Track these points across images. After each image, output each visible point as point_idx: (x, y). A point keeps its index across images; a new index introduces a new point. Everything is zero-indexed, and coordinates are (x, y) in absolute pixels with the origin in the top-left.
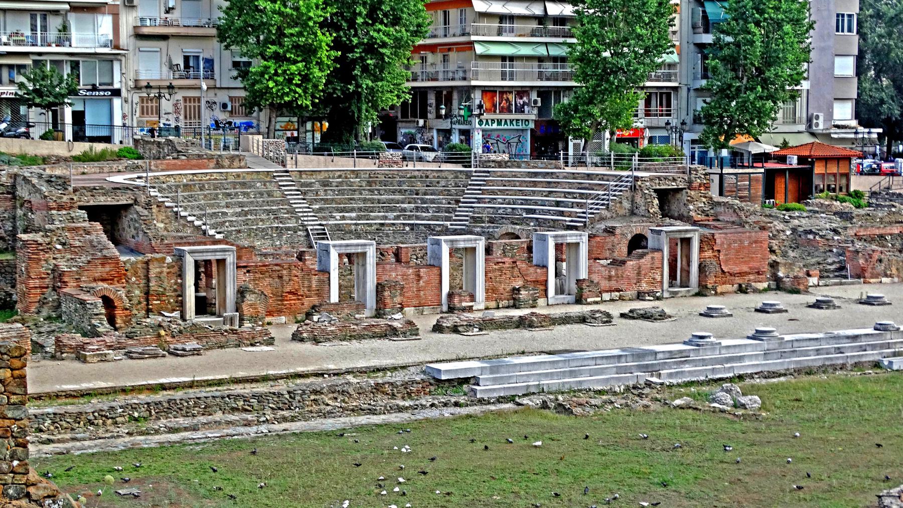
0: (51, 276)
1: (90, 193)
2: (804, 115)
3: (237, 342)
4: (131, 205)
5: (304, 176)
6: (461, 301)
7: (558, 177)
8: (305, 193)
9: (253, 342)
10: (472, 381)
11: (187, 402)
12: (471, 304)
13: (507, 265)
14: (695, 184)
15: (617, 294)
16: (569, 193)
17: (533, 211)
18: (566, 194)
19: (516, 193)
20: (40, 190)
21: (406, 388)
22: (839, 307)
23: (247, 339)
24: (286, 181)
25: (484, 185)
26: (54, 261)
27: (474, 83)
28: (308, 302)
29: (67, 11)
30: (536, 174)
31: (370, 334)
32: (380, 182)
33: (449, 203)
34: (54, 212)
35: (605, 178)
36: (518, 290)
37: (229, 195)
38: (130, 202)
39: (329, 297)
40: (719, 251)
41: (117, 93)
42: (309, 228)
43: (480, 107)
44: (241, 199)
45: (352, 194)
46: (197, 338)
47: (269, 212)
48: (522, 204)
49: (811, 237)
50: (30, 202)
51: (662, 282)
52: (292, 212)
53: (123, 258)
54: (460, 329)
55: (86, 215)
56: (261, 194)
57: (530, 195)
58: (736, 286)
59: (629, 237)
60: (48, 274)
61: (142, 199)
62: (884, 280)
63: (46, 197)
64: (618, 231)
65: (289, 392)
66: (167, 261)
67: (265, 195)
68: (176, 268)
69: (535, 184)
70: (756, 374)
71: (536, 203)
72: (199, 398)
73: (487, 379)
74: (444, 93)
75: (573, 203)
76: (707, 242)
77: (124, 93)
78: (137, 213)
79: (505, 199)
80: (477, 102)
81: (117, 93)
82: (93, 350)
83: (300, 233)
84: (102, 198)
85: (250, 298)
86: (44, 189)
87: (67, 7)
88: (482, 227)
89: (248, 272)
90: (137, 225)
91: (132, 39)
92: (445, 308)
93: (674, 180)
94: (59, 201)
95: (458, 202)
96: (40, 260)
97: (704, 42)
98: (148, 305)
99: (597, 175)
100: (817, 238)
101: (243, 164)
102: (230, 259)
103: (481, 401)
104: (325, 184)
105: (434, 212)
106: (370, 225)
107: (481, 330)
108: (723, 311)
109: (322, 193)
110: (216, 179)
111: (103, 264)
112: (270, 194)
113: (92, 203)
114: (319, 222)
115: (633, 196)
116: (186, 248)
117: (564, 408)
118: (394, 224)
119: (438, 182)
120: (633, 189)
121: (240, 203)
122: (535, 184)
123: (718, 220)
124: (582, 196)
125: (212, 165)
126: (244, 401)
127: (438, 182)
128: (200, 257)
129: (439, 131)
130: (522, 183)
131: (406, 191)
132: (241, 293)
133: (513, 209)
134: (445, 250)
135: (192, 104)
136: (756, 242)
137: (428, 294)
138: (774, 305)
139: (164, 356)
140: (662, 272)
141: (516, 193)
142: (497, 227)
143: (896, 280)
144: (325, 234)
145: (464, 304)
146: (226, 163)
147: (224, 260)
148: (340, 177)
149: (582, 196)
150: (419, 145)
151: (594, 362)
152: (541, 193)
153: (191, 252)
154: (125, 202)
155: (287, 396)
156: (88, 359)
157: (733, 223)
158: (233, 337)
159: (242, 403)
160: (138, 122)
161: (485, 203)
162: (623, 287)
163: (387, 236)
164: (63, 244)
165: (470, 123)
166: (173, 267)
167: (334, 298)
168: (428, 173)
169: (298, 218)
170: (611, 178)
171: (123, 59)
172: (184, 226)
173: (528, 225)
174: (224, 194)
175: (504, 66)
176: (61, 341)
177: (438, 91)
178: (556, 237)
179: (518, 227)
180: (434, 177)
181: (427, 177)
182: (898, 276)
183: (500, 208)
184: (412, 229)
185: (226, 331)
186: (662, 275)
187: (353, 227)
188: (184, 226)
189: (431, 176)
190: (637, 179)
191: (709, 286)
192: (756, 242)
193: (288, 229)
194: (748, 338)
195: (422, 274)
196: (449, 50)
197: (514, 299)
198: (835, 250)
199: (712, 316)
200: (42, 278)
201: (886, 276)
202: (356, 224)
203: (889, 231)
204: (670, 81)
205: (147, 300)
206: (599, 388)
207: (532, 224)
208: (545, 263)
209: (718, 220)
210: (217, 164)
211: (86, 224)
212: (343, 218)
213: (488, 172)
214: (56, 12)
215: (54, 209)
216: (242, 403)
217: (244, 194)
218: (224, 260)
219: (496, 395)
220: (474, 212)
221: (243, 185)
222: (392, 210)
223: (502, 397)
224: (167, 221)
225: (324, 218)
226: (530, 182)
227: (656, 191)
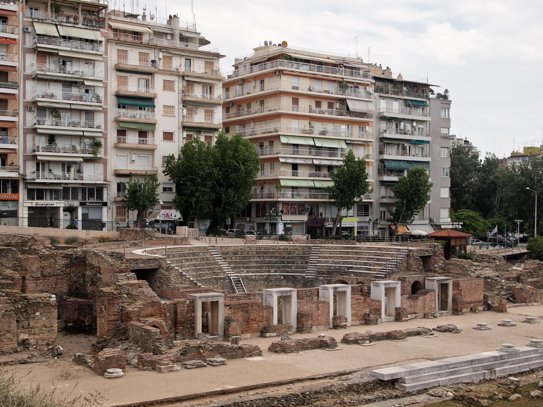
0: (120, 314)
1: (135, 262)
2: (428, 216)
3: (242, 355)
4: (158, 269)
5: (223, 249)
6: (341, 322)
7: (360, 249)
8: (225, 259)
9: (251, 354)
10: (400, 381)
11: (246, 404)
12: (345, 323)
13: (361, 301)
14: (437, 254)
15: (414, 315)
16: (370, 258)
17: (352, 268)
18: (368, 259)
19: (338, 258)
20: (108, 261)
21: (365, 387)
22: (539, 322)
23: (248, 353)
24: (214, 252)
25: (320, 254)
26: (122, 304)
27: (280, 200)
28: (261, 325)
29: (81, 162)
30: (348, 248)
31: (312, 346)
32: (263, 252)
33: (302, 264)
34: (117, 274)
35: (390, 250)
36: (369, 315)
37: (187, 260)
38: (157, 267)
39: (273, 321)
40: (461, 290)
41: (105, 204)
42: (231, 278)
43: (282, 211)
44: (194, 262)
45: (249, 259)
46: (220, 353)
47: (209, 269)
48: (343, 264)
49: (489, 280)
50: (99, 268)
51: (435, 308)
52: (221, 269)
53: (163, 302)
54: (360, 342)
55: (136, 276)
56: (203, 259)
57: (346, 259)
58: (469, 309)
59: (412, 282)
60: (119, 312)
61: (164, 265)
62: (534, 303)
63: (112, 265)
64: (407, 280)
65: (302, 394)
66: (187, 303)
67: (205, 260)
68: (191, 307)
69: (348, 253)
70: (540, 368)
71: (351, 263)
72: (252, 401)
73: (409, 379)
74: (261, 204)
75: (375, 264)
76: (456, 285)
77: (109, 204)
78: (162, 273)
79: (333, 261)
80: (280, 209)
81: (105, 204)
82: (165, 365)
83: (226, 281)
84: (142, 265)
85: (233, 324)
86: (110, 260)
87: (82, 160)
88: (324, 277)
89: (230, 308)
90: (162, 281)
91: (113, 177)
92: (331, 326)
93: (427, 251)
94: (120, 268)
95: (307, 263)
96: (114, 304)
97: (385, 180)
98: (176, 329)
99: (385, 248)
100: (493, 281)
101: (187, 242)
102: (221, 301)
103: (409, 394)
104: (235, 253)
105: (295, 268)
106: (262, 276)
107: (370, 342)
108: (488, 326)
109: (234, 258)
110: (179, 251)
111: (152, 306)
112: (207, 259)
113: (136, 268)
114: (235, 275)
115: (408, 260)
116: (197, 295)
117: (473, 400)
118: (275, 275)
119: (294, 252)
120: (408, 256)
121: (194, 264)
122: (348, 253)
123: (450, 273)
124: (378, 260)
125: (172, 243)
126: (278, 401)
127: (294, 252)
128: (204, 300)
129: (257, 223)
130: (341, 253)
131: (278, 256)
132: (228, 321)
133: (340, 267)
134: (331, 292)
135: (121, 210)
136: (478, 285)
137: (323, 319)
138: (510, 322)
139: (205, 366)
140: (435, 302)
141: (338, 258)
142: (333, 277)
143: (540, 303)
144: (240, 281)
145: (343, 324)
146: (179, 242)
147: (217, 302)
148: (241, 249)
149: (378, 260)
150: (235, 230)
151: (460, 365)
152: (353, 258)
153: (200, 298)
154: (154, 267)
155: (301, 396)
156: (162, 370)
157: (460, 274)
158: (240, 352)
159: (276, 402)
160: (115, 219)
161: (322, 263)
162: (417, 311)
163: (271, 281)
164: (128, 294)
165: (277, 220)
166: (190, 306)
167: (275, 322)
168: (288, 247)
169: (224, 272)
170: (393, 250)
171: (108, 186)
172: (185, 280)
173: (350, 275)
174: (185, 259)
175: (293, 191)
176: (142, 358)
177: (258, 203)
178: (385, 284)
179: (345, 277)
180: (291, 249)
181: (287, 249)
182: (540, 302)
183: (332, 266)
184: (284, 278)
185: (236, 348)
186: (435, 304)
187: (254, 277)
188: (185, 280)
189: (289, 249)
190: (410, 251)
191: (459, 310)
192: (478, 285)
193: (221, 279)
194: (527, 345)
195: (320, 307)
196: (264, 183)
197: (366, 320)
198: (505, 287)
199: (481, 330)
200: (115, 315)
201: (535, 302)
202: (255, 275)
203: (511, 276)
204: (317, 198)
205: (175, 327)
206: (467, 381)
207: (352, 275)
208: (379, 299)
209: (450, 273)
210: (175, 242)
211: (136, 281)
212: (248, 272)
213: (321, 246)
214: (75, 163)
215: (117, 272)
216: (276, 402)
217: (195, 259)
218: (217, 302)
219: (416, 389)
220: (318, 269)
221: (194, 254)
222: (272, 267)
223: (419, 390)
224: (176, 278)
225: (239, 272)
226: (345, 252)
227: (421, 257)
